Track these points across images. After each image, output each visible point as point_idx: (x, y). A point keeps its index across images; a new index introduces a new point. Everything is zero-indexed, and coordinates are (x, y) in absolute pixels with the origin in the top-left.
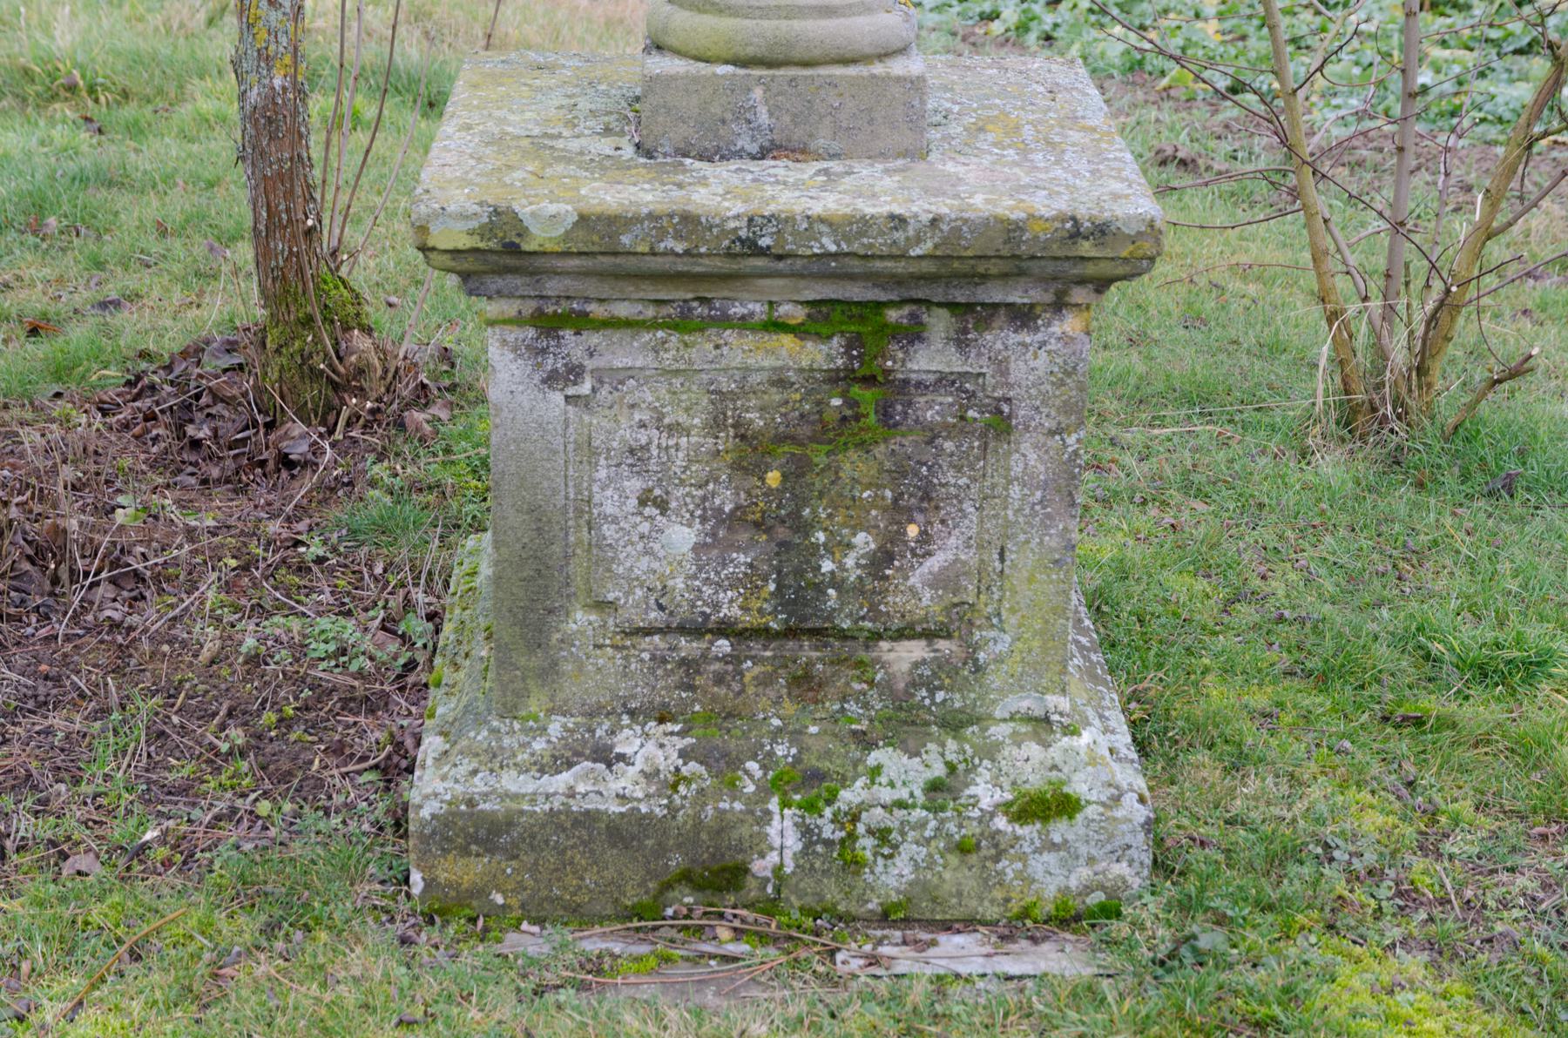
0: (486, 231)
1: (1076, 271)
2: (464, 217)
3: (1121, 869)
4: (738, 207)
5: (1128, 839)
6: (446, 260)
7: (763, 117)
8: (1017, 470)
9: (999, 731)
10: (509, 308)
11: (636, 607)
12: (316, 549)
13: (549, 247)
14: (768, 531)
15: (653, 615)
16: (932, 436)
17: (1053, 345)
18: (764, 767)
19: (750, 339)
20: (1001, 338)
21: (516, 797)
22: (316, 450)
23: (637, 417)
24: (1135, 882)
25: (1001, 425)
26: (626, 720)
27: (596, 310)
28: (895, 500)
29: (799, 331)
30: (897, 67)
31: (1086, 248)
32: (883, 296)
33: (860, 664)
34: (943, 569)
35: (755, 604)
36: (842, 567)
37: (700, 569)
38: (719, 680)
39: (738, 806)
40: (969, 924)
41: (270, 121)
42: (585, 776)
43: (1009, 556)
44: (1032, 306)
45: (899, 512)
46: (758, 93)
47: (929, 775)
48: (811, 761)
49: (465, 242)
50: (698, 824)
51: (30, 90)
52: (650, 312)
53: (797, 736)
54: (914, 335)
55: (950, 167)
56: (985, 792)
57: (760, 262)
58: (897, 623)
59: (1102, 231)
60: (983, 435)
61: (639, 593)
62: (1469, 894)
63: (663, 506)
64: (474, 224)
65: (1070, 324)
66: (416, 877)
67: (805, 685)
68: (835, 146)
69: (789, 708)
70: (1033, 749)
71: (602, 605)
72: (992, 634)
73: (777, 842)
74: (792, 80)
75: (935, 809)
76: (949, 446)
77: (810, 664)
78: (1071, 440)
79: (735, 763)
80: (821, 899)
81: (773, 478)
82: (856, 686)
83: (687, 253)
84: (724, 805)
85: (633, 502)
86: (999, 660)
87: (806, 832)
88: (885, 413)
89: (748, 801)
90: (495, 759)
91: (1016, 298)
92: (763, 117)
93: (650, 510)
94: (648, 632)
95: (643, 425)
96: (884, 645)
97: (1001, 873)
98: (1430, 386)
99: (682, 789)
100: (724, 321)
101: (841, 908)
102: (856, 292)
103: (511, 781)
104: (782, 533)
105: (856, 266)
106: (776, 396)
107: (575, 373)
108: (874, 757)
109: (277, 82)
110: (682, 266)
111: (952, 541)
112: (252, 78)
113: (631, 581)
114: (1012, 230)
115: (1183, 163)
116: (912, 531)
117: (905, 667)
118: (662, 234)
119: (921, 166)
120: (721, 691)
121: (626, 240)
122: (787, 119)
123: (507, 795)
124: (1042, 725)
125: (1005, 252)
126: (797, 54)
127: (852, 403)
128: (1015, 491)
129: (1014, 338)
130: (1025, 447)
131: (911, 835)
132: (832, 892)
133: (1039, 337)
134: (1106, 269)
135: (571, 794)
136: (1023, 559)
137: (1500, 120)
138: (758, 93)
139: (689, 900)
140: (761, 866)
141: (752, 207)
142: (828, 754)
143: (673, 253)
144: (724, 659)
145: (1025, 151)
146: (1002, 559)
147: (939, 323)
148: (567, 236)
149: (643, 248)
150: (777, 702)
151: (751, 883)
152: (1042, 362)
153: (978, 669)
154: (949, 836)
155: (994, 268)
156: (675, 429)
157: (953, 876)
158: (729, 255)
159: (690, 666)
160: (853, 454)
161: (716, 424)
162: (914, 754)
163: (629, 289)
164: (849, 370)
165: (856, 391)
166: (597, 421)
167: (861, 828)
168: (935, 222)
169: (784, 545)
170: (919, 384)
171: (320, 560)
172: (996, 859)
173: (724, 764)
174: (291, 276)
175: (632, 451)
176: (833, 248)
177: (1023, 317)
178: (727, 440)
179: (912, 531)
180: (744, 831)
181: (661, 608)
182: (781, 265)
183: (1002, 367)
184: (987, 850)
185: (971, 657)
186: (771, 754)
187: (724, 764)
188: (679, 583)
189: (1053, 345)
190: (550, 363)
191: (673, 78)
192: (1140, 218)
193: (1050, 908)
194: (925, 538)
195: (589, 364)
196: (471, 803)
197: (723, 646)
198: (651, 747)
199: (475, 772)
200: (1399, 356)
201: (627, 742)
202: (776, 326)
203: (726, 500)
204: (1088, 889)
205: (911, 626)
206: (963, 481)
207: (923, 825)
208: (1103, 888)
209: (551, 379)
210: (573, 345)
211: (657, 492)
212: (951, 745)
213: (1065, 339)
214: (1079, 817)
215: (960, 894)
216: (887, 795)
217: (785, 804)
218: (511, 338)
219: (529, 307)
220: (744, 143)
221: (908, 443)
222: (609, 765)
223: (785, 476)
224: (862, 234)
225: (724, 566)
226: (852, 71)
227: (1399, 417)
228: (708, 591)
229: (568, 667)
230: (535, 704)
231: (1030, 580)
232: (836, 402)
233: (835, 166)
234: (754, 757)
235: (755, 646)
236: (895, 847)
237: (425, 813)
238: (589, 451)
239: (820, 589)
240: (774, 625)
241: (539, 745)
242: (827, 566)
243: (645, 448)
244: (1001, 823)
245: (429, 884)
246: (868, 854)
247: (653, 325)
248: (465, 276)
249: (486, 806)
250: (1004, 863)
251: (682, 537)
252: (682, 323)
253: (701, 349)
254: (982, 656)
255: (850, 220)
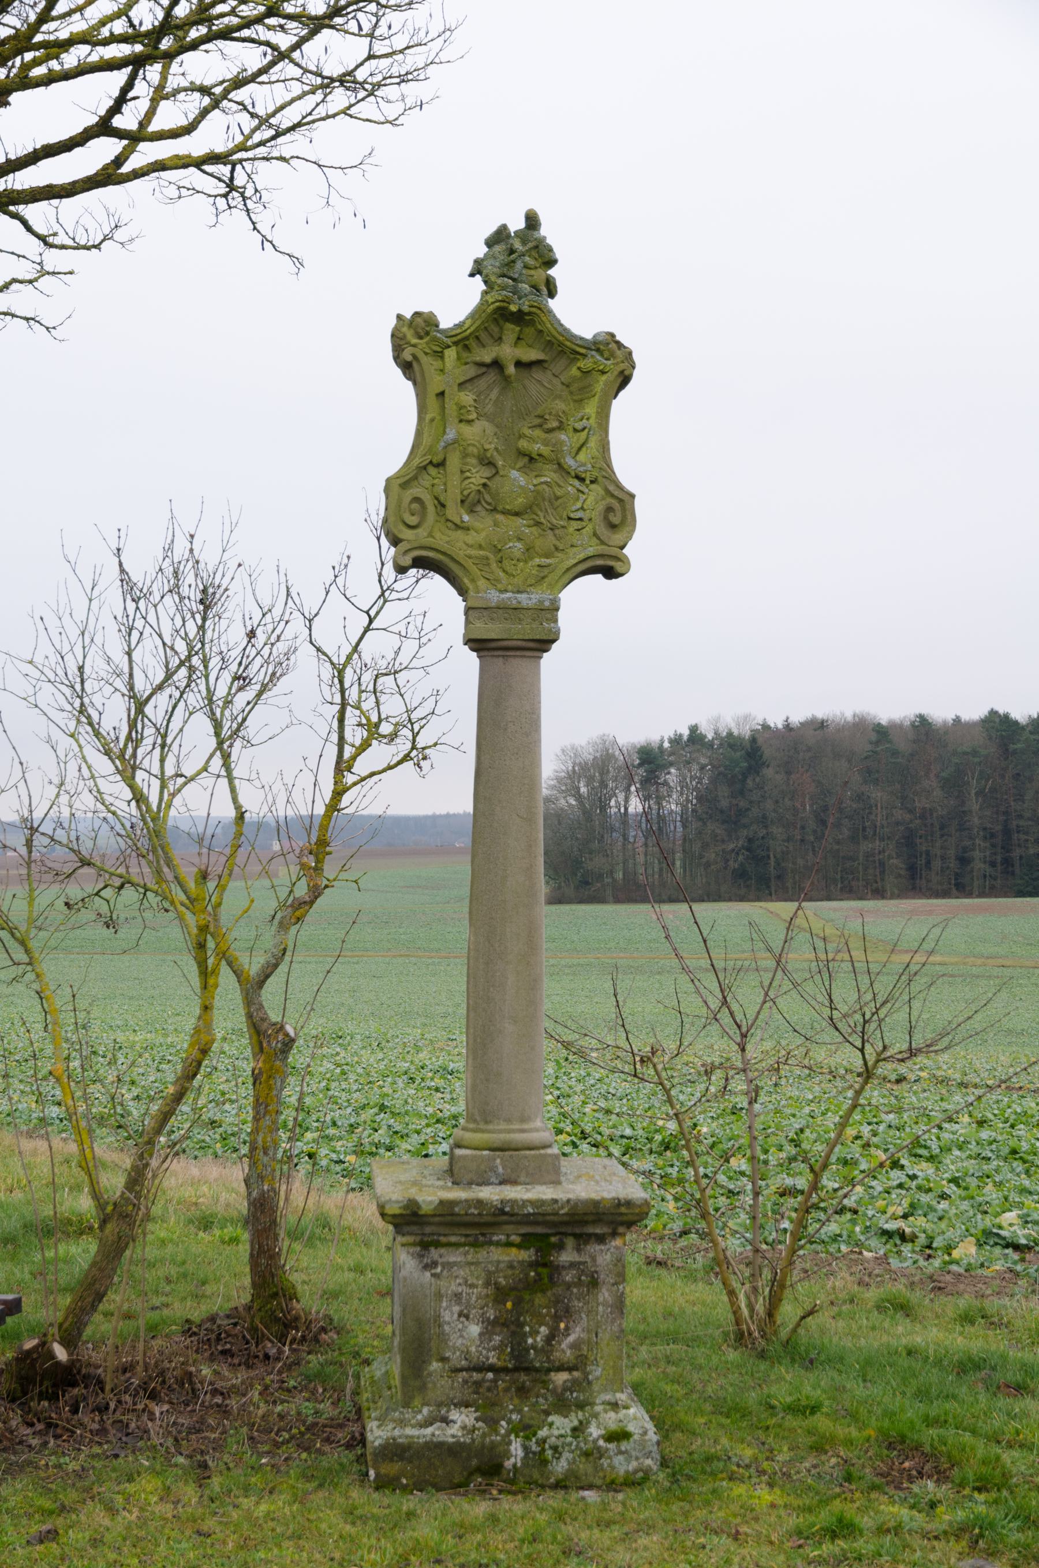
0: (406, 1207)
1: (620, 1219)
2: (398, 1202)
3: (649, 1462)
4: (496, 1197)
5: (651, 1448)
6: (390, 1219)
7: (500, 1170)
8: (601, 1299)
9: (598, 1408)
10: (410, 1239)
11: (456, 1359)
12: (292, 1383)
13: (429, 1212)
14: (507, 1327)
15: (463, 1362)
16: (569, 1286)
17: (612, 1250)
18: (508, 1423)
19: (500, 1250)
20: (594, 1248)
21: (412, 1437)
22: (280, 1352)
23: (458, 1281)
24: (655, 1468)
25: (594, 1283)
26: (452, 1407)
27: (443, 1239)
28: (556, 1312)
29: (519, 1246)
30: (549, 1151)
31: (623, 1210)
32: (549, 1231)
33: (544, 1382)
34: (575, 1341)
35: (503, 1357)
36: (535, 1341)
37: (481, 1343)
38: (489, 1390)
39: (498, 1438)
40: (590, 1487)
41: (262, 1205)
42: (438, 1428)
43: (600, 1335)
44: (604, 1234)
45: (557, 1319)
46: (498, 1161)
47: (572, 1425)
48: (527, 1421)
49: (398, 1211)
50: (483, 1445)
51: (71, 1229)
52: (463, 1240)
53: (520, 1411)
54: (561, 1247)
55: (571, 1186)
56: (594, 1431)
57: (505, 1218)
58: (557, 1364)
59: (628, 1203)
60: (588, 1286)
61: (458, 1353)
62: (784, 1470)
63: (467, 1317)
64: (401, 1205)
65: (618, 1242)
66: (372, 1473)
67: (522, 1392)
68: (527, 1180)
69: (516, 1401)
70: (612, 1414)
71: (443, 1359)
72: (594, 1367)
73: (514, 1453)
74: (511, 1156)
75: (575, 1437)
76: (575, 1290)
77: (524, 1382)
78: (621, 1287)
79: (496, 1422)
80: (531, 1477)
81: (509, 1305)
82: (542, 1391)
83: (479, 1214)
84: (493, 1438)
85: (456, 1316)
86: (597, 1379)
87: (526, 1448)
88: (551, 1278)
89: (503, 1436)
90: (402, 1423)
91: (598, 1231)
92: (500, 1170)
93: (462, 1319)
94: (461, 1370)
95: (460, 1284)
96: (552, 1374)
97: (602, 1465)
98: (775, 1323)
99: (477, 1432)
100: (491, 1243)
101: (540, 1482)
102: (539, 1230)
103: (409, 1431)
104: (513, 1328)
105: (540, 1219)
106: (510, 1272)
107: (435, 1264)
108: (550, 1419)
109: (266, 1188)
110: (477, 1220)
111: (578, 1329)
112: (255, 1185)
113: (455, 1349)
114: (596, 1203)
115: (659, 1263)
116: (562, 1325)
117: (561, 1382)
118: (470, 1207)
119: (559, 1187)
120: (489, 1394)
121: (457, 1209)
122: (509, 1170)
123: (407, 1437)
124: (615, 1406)
125: (594, 1211)
126: (513, 1146)
127: (538, 1274)
128: (601, 1308)
129: (598, 1247)
130: (604, 1290)
131: (567, 1448)
132: (536, 1475)
133: (607, 1246)
134: (630, 1218)
135: (433, 1435)
136: (605, 1336)
137: (823, 1242)
138: (498, 1161)
139: (480, 1480)
140: (508, 1464)
141: (502, 1197)
142: (532, 1418)
143: (473, 1214)
144: (491, 1381)
145: (597, 1182)
146: (597, 1336)
147: (570, 1242)
148: (435, 1209)
149: (462, 1212)
150: (511, 1399)
151: (504, 1472)
152: (608, 1257)
153: (589, 1383)
154: (581, 1449)
155: (590, 1218)
156: (472, 1286)
157: (583, 1467)
158: (494, 1215)
159: (478, 1384)
160: (539, 1295)
161: (487, 1284)
162: (566, 1417)
163: (456, 1231)
164: (537, 1261)
165: (540, 1270)
166: (442, 1283)
167: (547, 1446)
168: (568, 1201)
169: (513, 1333)
170: (563, 1267)
171: (295, 1388)
172: (600, 1459)
173: (492, 1423)
174: (267, 1275)
175: (456, 1295)
176: (531, 1211)
177: (601, 1239)
178: (490, 1291)
179: (562, 1325)
180: (501, 1448)
181: (466, 1359)
182: (513, 1219)
183: (594, 1259)
184: (596, 1455)
185: (586, 1378)
186: (510, 1418)
187: (492, 1423)
188: (473, 1349)
189: (612, 1250)
190: (425, 1260)
191: (467, 1156)
192: (642, 1199)
193: (622, 1480)
194: (567, 1328)
195: (440, 1260)
196: (394, 1439)
197: (490, 1375)
198: (463, 1417)
199: (394, 1428)
200: (760, 1308)
201: (454, 1415)
202: (509, 1244)
203: (491, 1314)
204: (636, 1471)
205: (563, 1365)
206: (581, 1305)
207: (570, 1444)
208: (641, 1470)
209: (426, 1267)
210: (434, 1253)
211: (465, 1311)
212: (580, 1413)
213: (617, 1248)
214: (631, 1440)
215: (586, 1475)
216: (556, 1433)
217: (517, 1436)
218: (411, 1250)
219: (418, 1239)
220: (493, 1180)
221: (559, 1290)
222: (447, 1424)
223: (514, 1305)
224: (542, 1205)
225: (491, 1341)
226: (532, 1152)
227: (762, 1337)
228: (484, 1352)
229: (430, 1385)
230: (417, 1402)
231: (608, 1345)
232: (532, 1274)
233: (529, 1187)
234: (503, 1419)
235: (502, 1375)
236: (560, 1454)
237: (377, 1444)
238: (439, 1296)
239: (527, 1350)
240: (510, 1366)
241: (419, 1417)
242: (530, 1341)
243: (461, 1294)
244: (601, 1443)
245: (377, 1475)
246: (550, 1457)
247: (464, 1245)
248: (396, 1226)
249: (400, 1440)
250: (603, 1460)
251: (475, 1330)
252: (475, 1244)
253: (482, 1254)
254: (590, 1377)
255: (538, 1201)
